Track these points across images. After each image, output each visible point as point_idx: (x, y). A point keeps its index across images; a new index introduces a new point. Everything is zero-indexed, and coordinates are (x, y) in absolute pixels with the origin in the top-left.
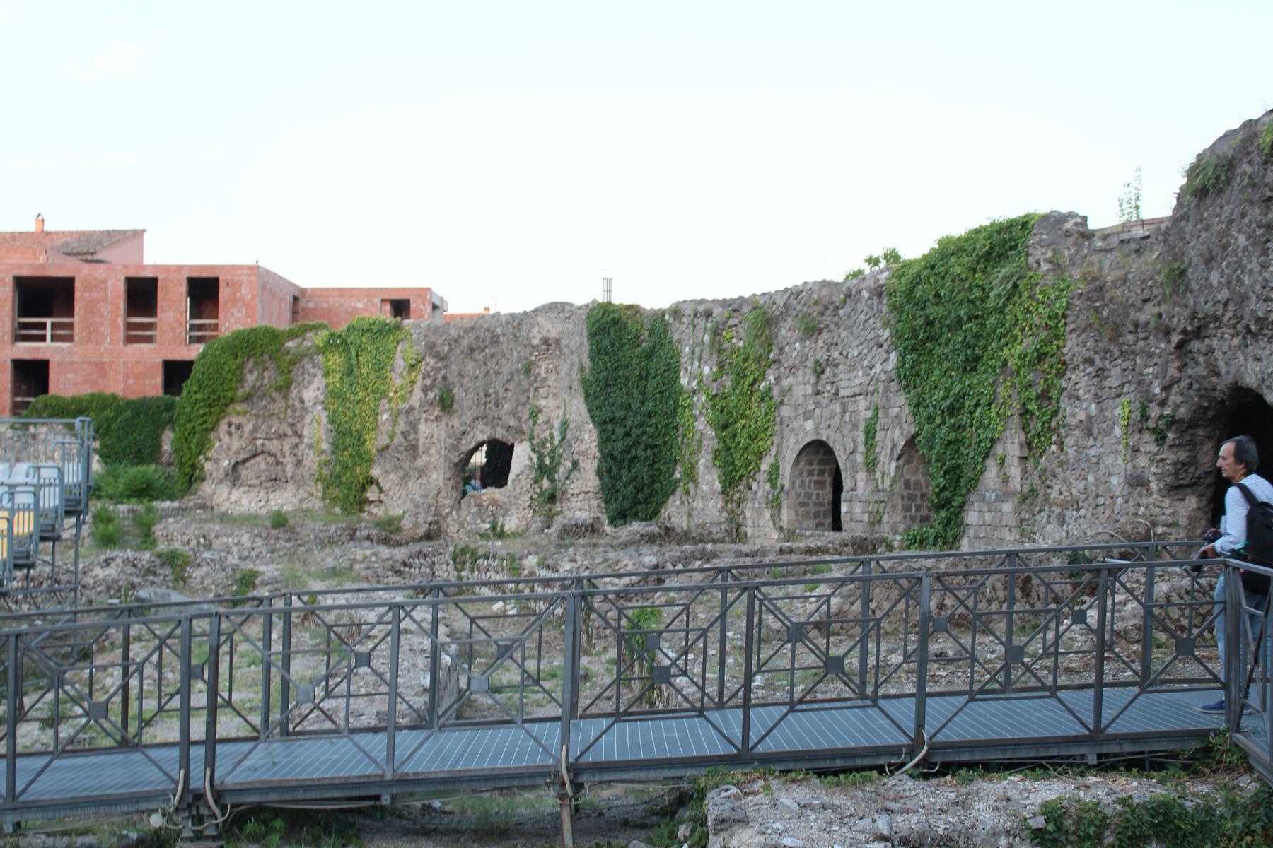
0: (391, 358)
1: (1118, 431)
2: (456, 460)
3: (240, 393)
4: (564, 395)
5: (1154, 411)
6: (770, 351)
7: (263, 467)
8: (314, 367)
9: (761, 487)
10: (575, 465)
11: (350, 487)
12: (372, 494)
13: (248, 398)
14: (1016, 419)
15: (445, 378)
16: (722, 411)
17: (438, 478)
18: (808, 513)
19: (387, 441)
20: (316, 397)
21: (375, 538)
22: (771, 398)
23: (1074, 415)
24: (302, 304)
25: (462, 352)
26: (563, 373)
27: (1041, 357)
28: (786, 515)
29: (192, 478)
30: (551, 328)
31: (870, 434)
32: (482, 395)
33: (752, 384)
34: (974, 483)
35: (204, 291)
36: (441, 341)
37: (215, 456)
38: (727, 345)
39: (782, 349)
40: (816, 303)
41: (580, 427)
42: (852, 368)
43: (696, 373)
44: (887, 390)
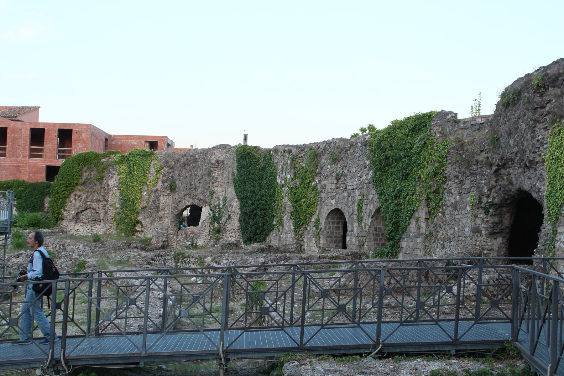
0: (149, 167)
1: (468, 208)
2: (176, 213)
3: (81, 181)
4: (225, 186)
5: (484, 200)
6: (317, 169)
7: (90, 214)
8: (114, 170)
9: (311, 229)
10: (229, 217)
11: (129, 224)
12: (138, 228)
13: (84, 184)
14: (424, 201)
15: (172, 177)
16: (295, 195)
17: (168, 221)
18: (332, 241)
19: (146, 204)
20: (115, 184)
21: (139, 247)
22: (317, 189)
23: (449, 201)
24: (109, 142)
25: (180, 165)
26: (225, 176)
27: (436, 175)
28: (322, 241)
29: (58, 219)
30: (220, 156)
31: (360, 206)
32: (189, 185)
33: (308, 183)
34: (405, 229)
35: (66, 135)
36: (171, 160)
37: (69, 209)
38: (298, 165)
39: (322, 168)
40: (338, 148)
41: (232, 200)
42: (353, 177)
43: (284, 177)
44: (368, 187)
